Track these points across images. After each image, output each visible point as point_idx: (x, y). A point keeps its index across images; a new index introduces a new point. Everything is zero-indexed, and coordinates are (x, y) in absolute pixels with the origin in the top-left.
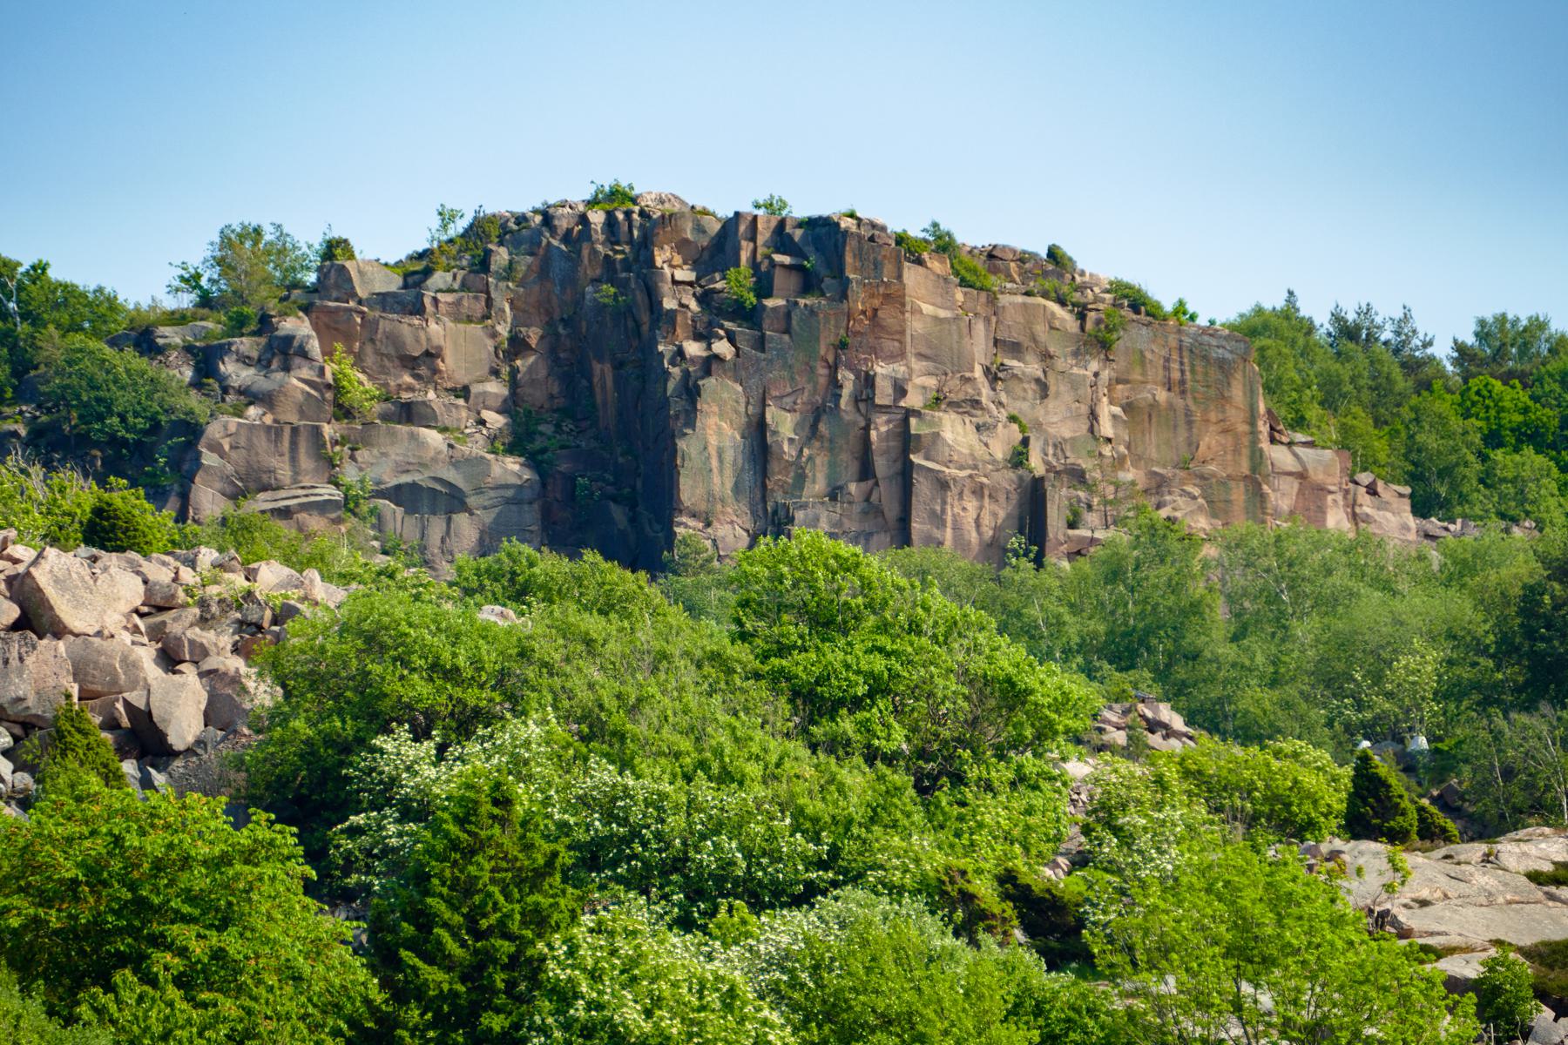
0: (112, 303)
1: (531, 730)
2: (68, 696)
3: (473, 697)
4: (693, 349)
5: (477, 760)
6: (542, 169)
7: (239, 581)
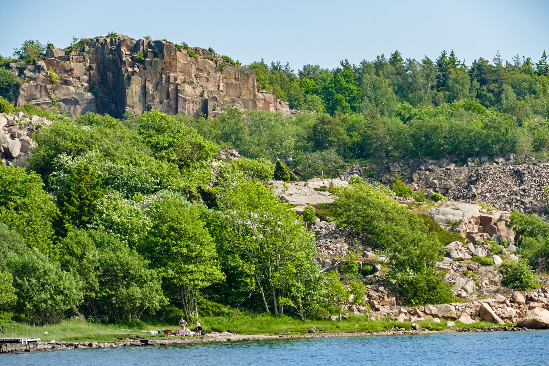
4: (130, 69)
5: (81, 161)
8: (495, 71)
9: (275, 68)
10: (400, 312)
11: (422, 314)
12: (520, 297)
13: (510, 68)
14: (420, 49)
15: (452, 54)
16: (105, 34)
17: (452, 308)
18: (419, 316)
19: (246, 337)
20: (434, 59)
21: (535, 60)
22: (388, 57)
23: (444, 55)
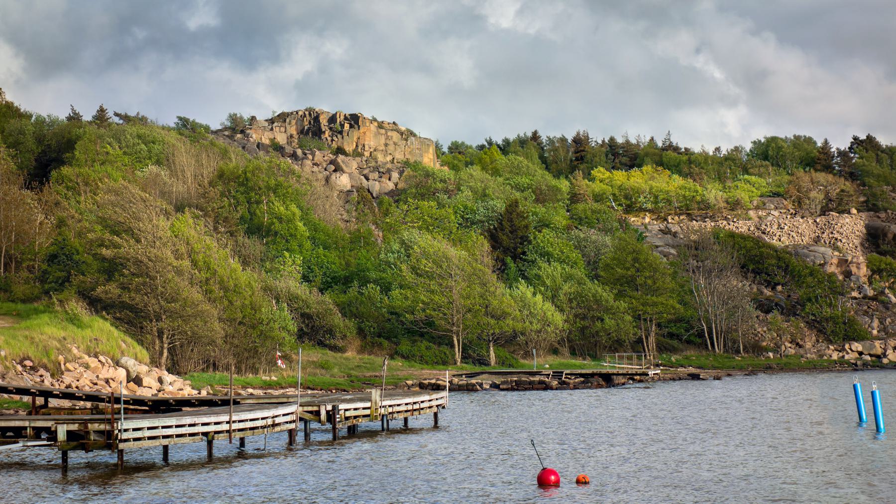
16: (303, 108)
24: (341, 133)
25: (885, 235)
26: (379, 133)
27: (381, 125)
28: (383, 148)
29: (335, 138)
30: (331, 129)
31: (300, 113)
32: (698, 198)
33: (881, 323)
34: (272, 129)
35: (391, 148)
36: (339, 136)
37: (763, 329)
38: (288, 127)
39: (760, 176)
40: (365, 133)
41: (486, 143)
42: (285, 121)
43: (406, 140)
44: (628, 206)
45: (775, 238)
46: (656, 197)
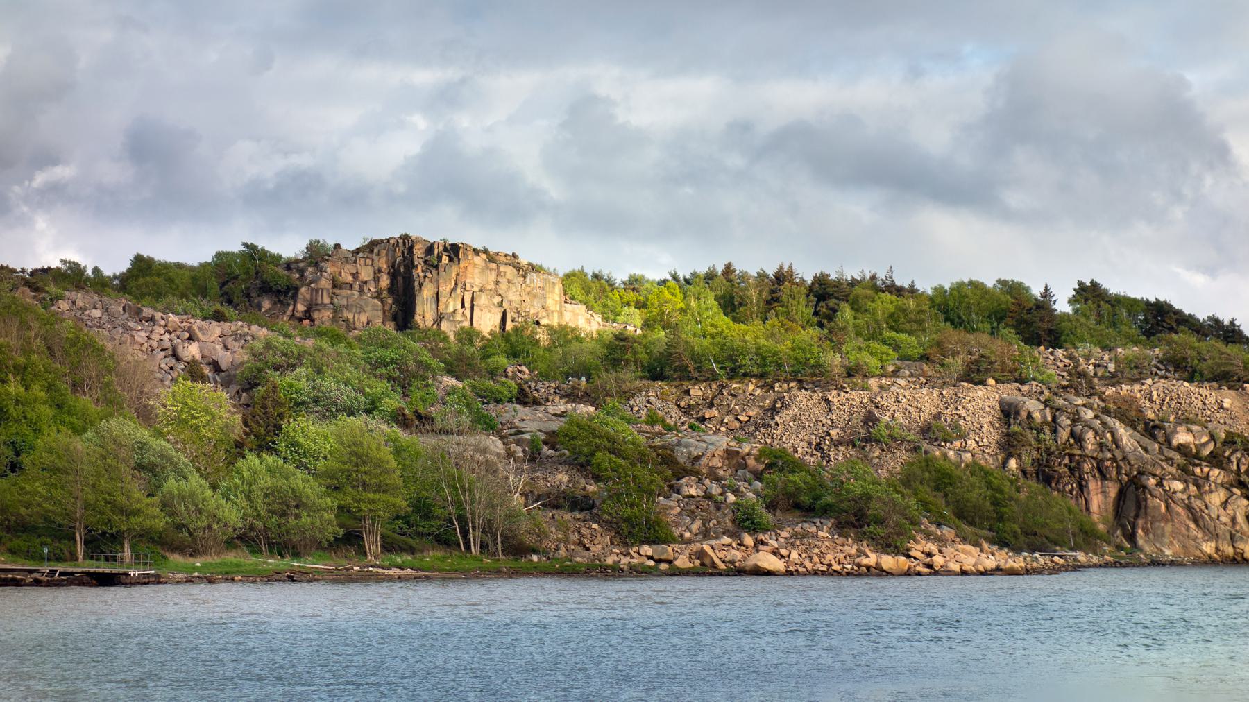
0: (280, 257)
1: (302, 371)
2: (1146, 532)
3: (291, 361)
4: (366, 274)
5: (288, 378)
6: (390, 230)
7: (246, 330)
8: (838, 284)
9: (596, 276)
10: (612, 552)
11: (635, 555)
12: (748, 540)
13: (854, 283)
14: (40, 267)
15: (791, 267)
16: (397, 235)
17: (670, 549)
18: (632, 557)
19: (386, 572)
20: (771, 272)
21: (881, 275)
22: (720, 269)
23: (781, 268)
24: (436, 267)
25: (1017, 413)
26: (488, 268)
27: (492, 258)
28: (492, 286)
29: (428, 274)
30: (425, 262)
31: (392, 241)
32: (812, 361)
33: (704, 524)
34: (355, 262)
35: (503, 287)
36: (434, 271)
37: (558, 530)
38: (376, 258)
39: (910, 333)
40: (466, 268)
41: (669, 278)
42: (372, 251)
43: (524, 277)
44: (733, 370)
45: (888, 414)
46: (764, 359)
